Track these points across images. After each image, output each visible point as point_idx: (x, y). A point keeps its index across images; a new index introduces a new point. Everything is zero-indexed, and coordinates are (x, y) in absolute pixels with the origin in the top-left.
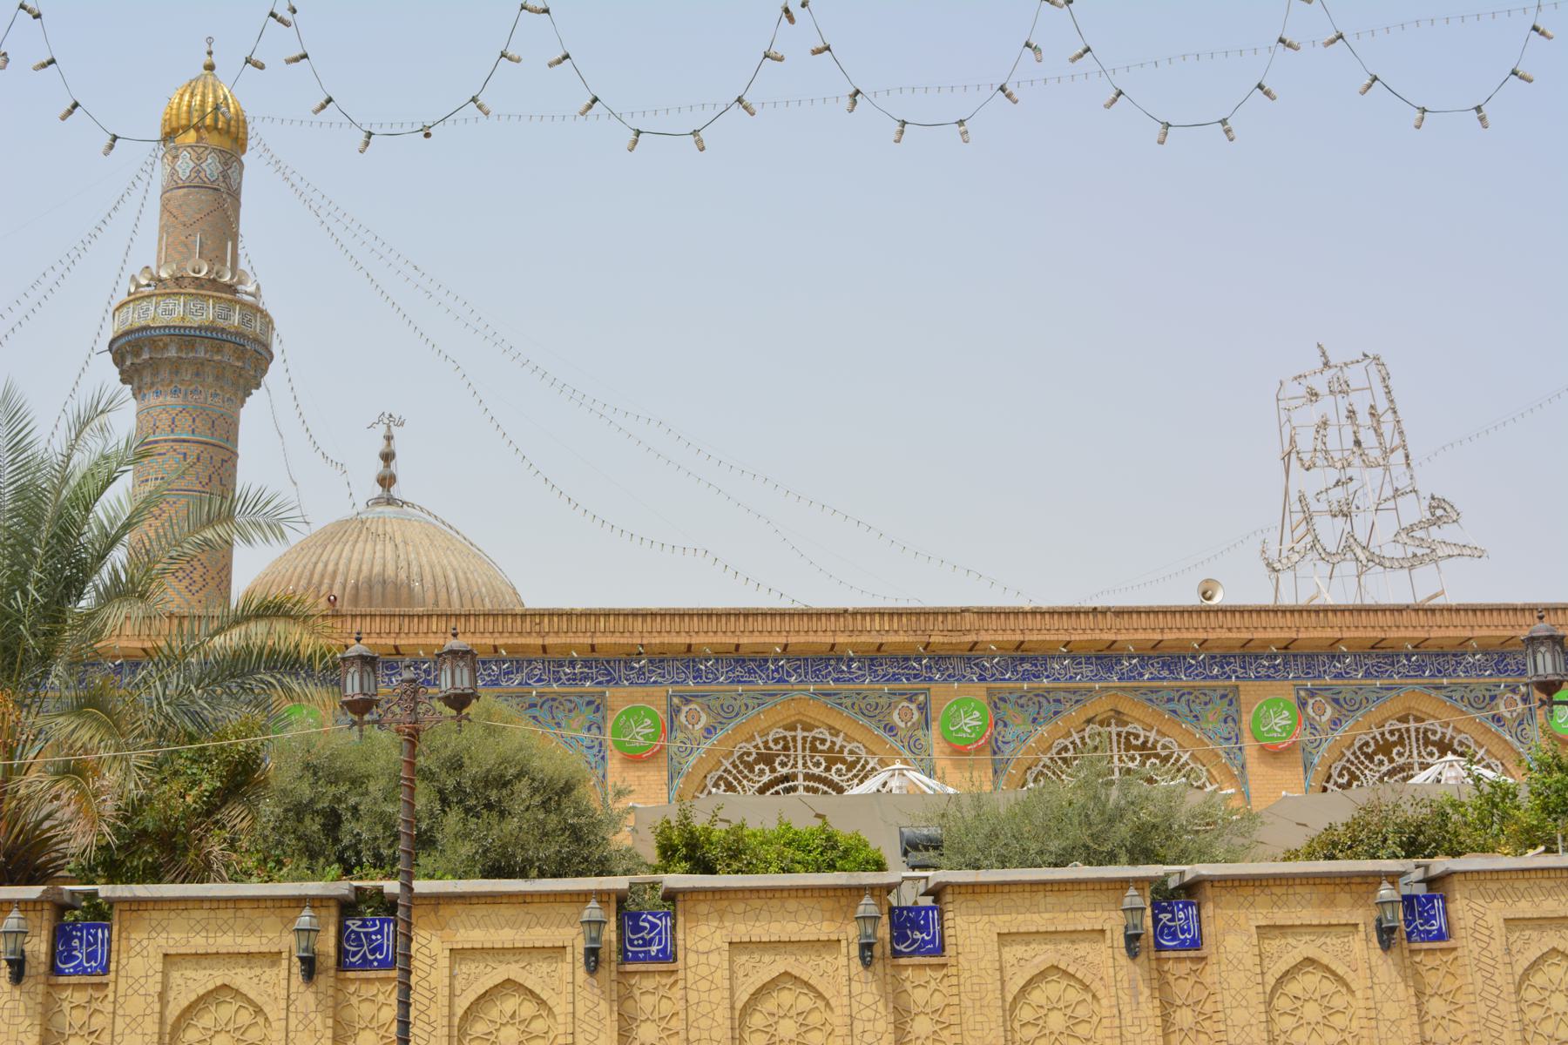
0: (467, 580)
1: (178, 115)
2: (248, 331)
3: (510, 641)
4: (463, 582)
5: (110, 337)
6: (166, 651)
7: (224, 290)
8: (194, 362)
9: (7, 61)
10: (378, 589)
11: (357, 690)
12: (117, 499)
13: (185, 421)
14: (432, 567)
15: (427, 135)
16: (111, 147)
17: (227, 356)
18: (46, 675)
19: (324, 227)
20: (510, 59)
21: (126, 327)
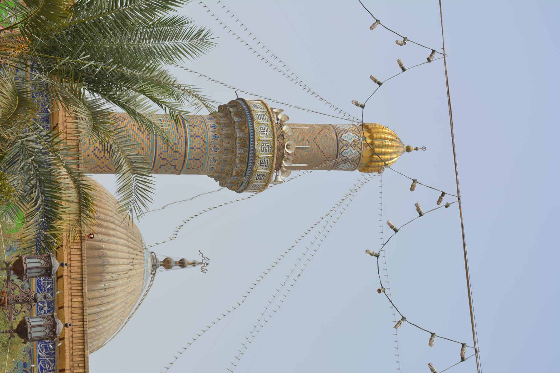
0: (107, 317)
1: (379, 132)
2: (254, 178)
3: (67, 348)
4: (105, 314)
5: (246, 99)
6: (56, 140)
7: (278, 162)
8: (234, 146)
9: (401, 45)
10: (99, 262)
11: (29, 265)
12: (148, 107)
13: (198, 143)
14: (114, 294)
15: (379, 291)
16: (357, 105)
17: (239, 166)
18: (40, 70)
19: (320, 220)
20: (431, 339)
21: (252, 108)
